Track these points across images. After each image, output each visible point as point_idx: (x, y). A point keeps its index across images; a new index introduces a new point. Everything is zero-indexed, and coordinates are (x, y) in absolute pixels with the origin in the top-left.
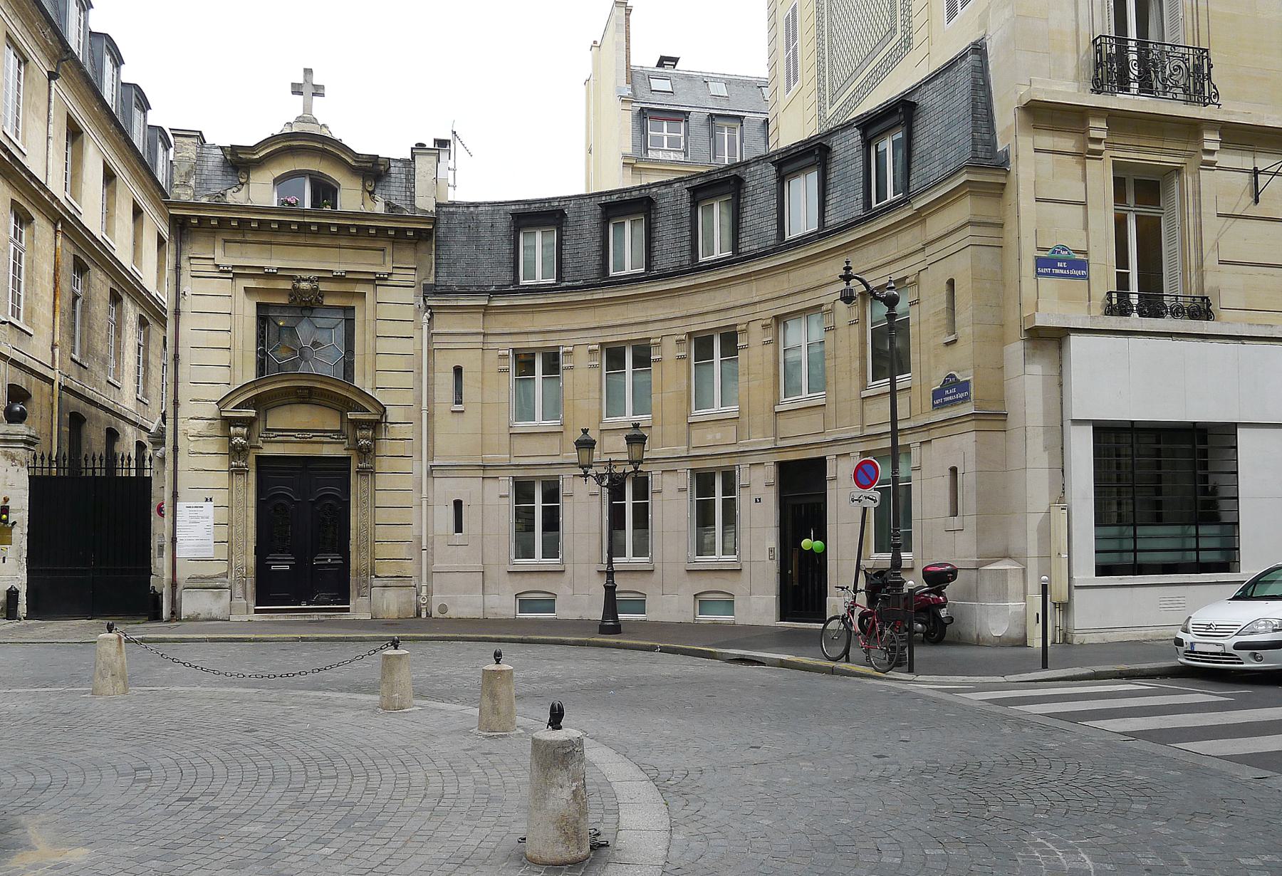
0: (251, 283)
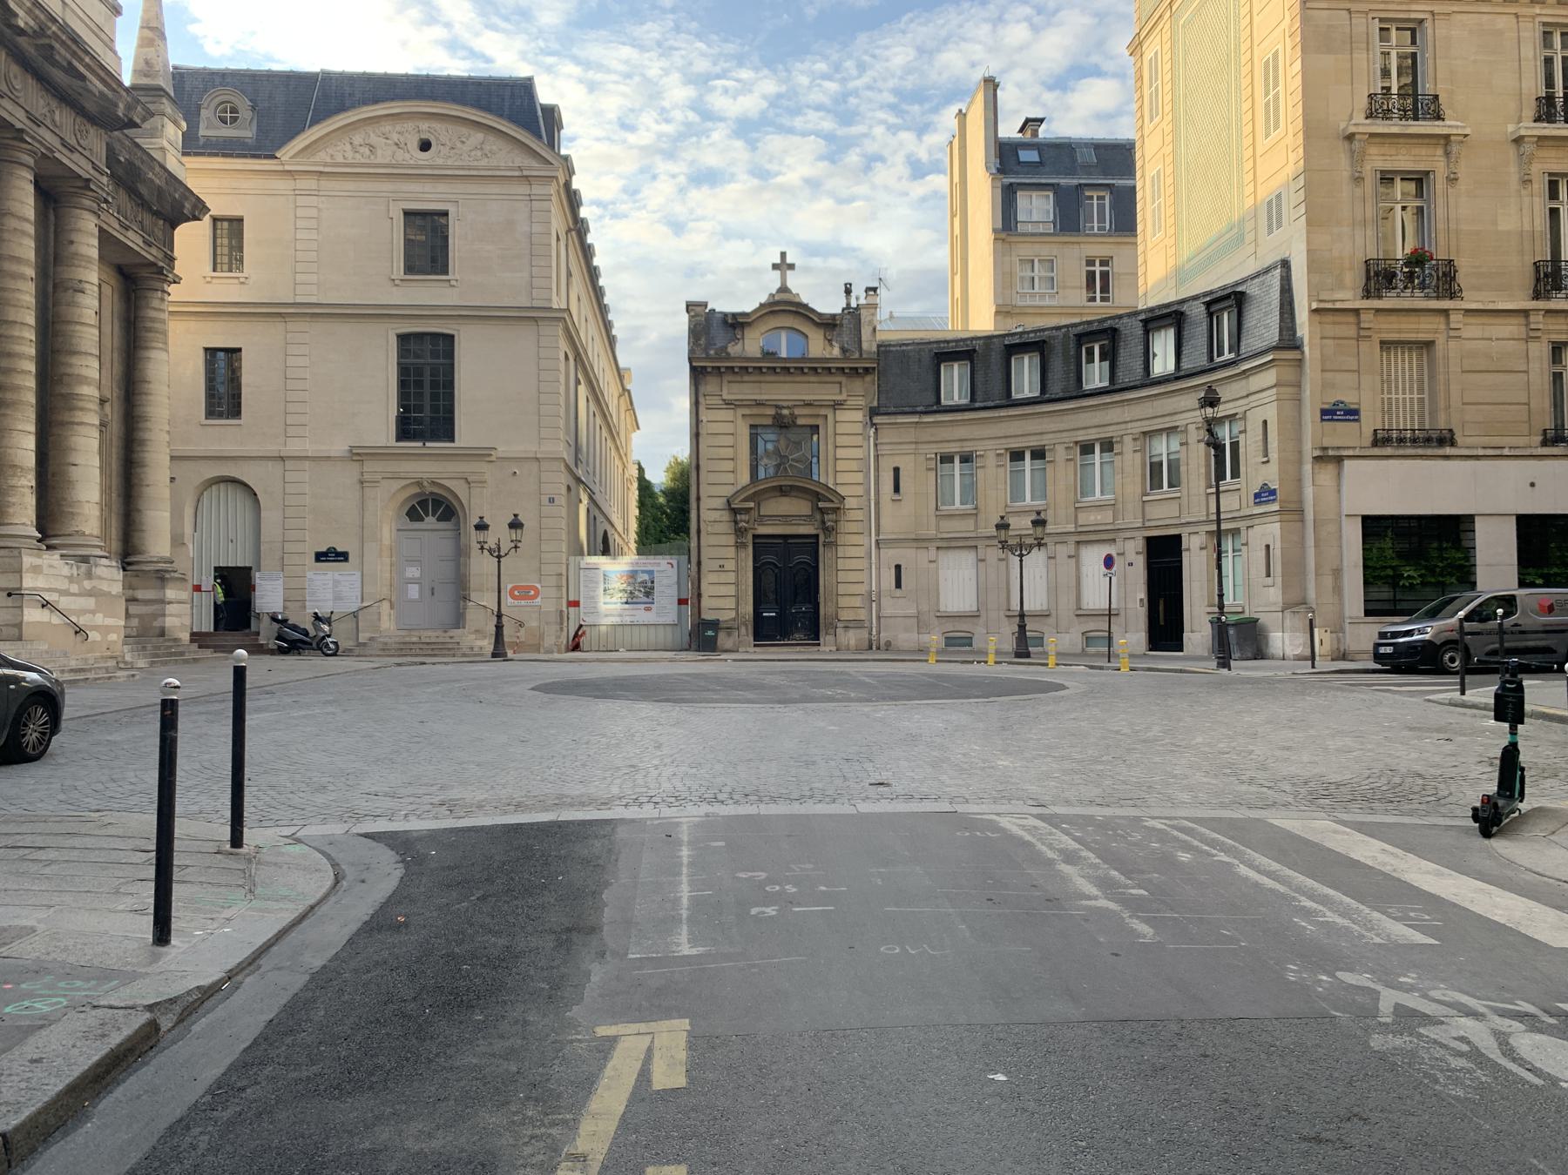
0: (747, 411)
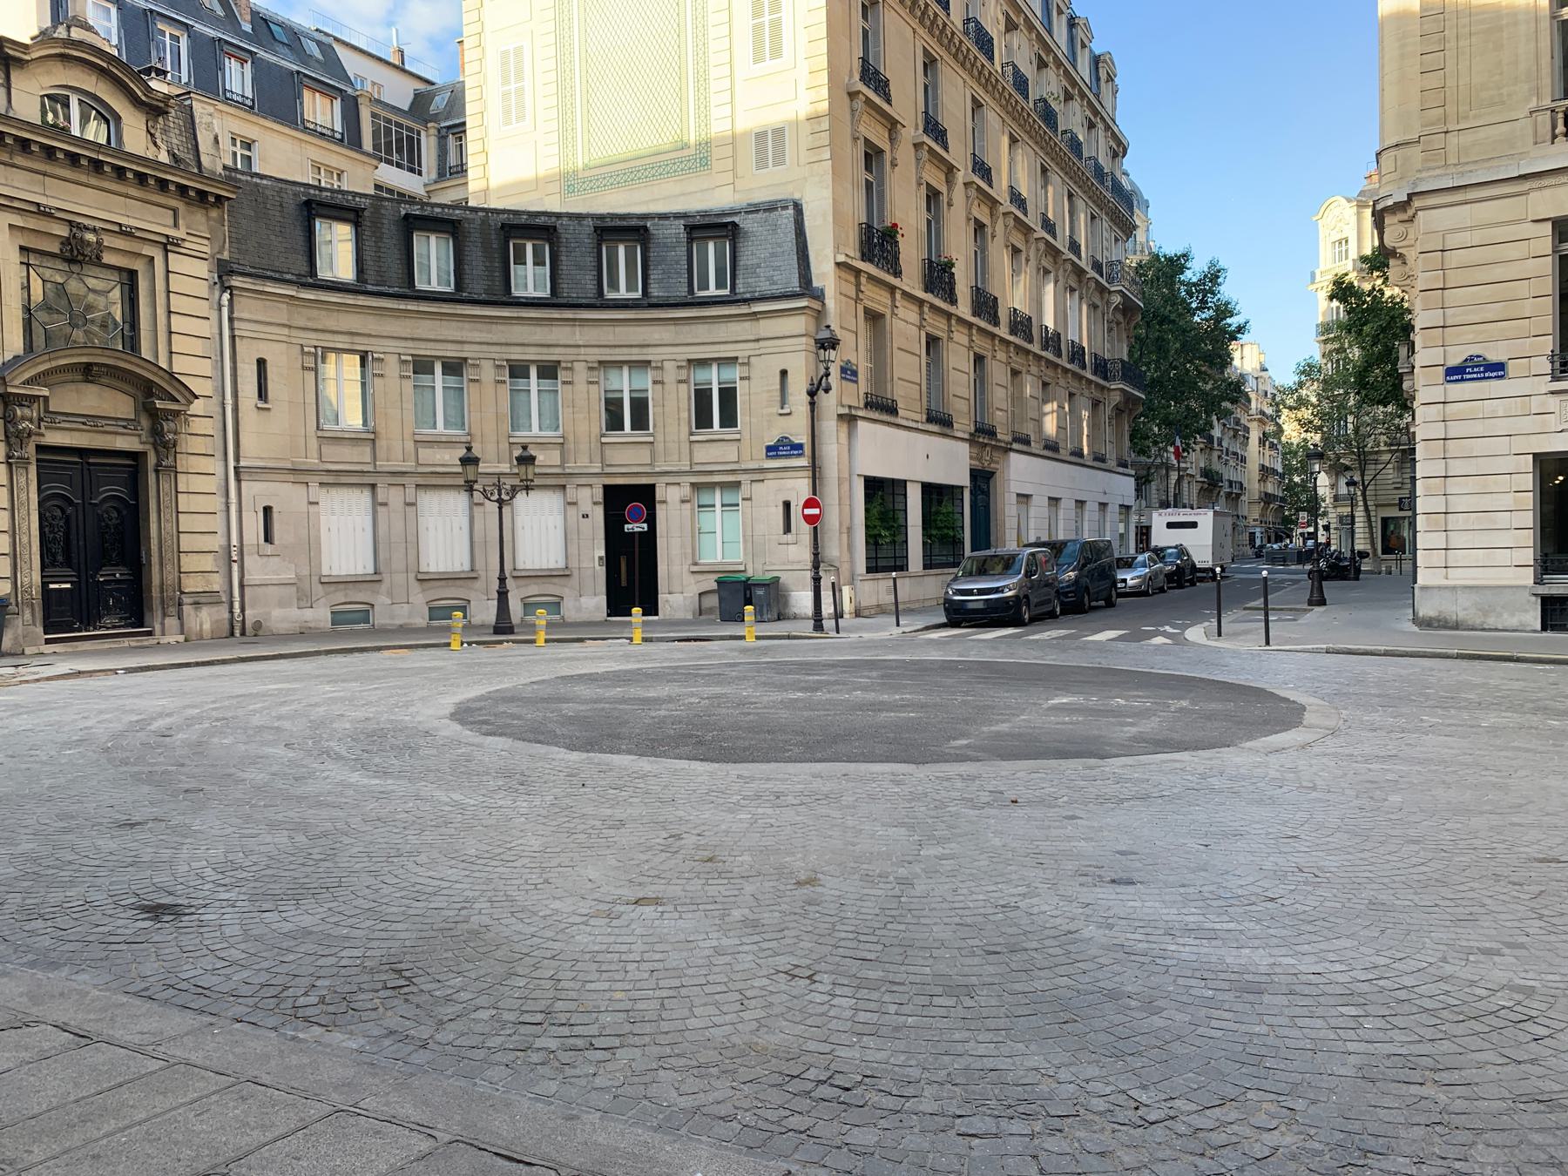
0: (18, 220)
